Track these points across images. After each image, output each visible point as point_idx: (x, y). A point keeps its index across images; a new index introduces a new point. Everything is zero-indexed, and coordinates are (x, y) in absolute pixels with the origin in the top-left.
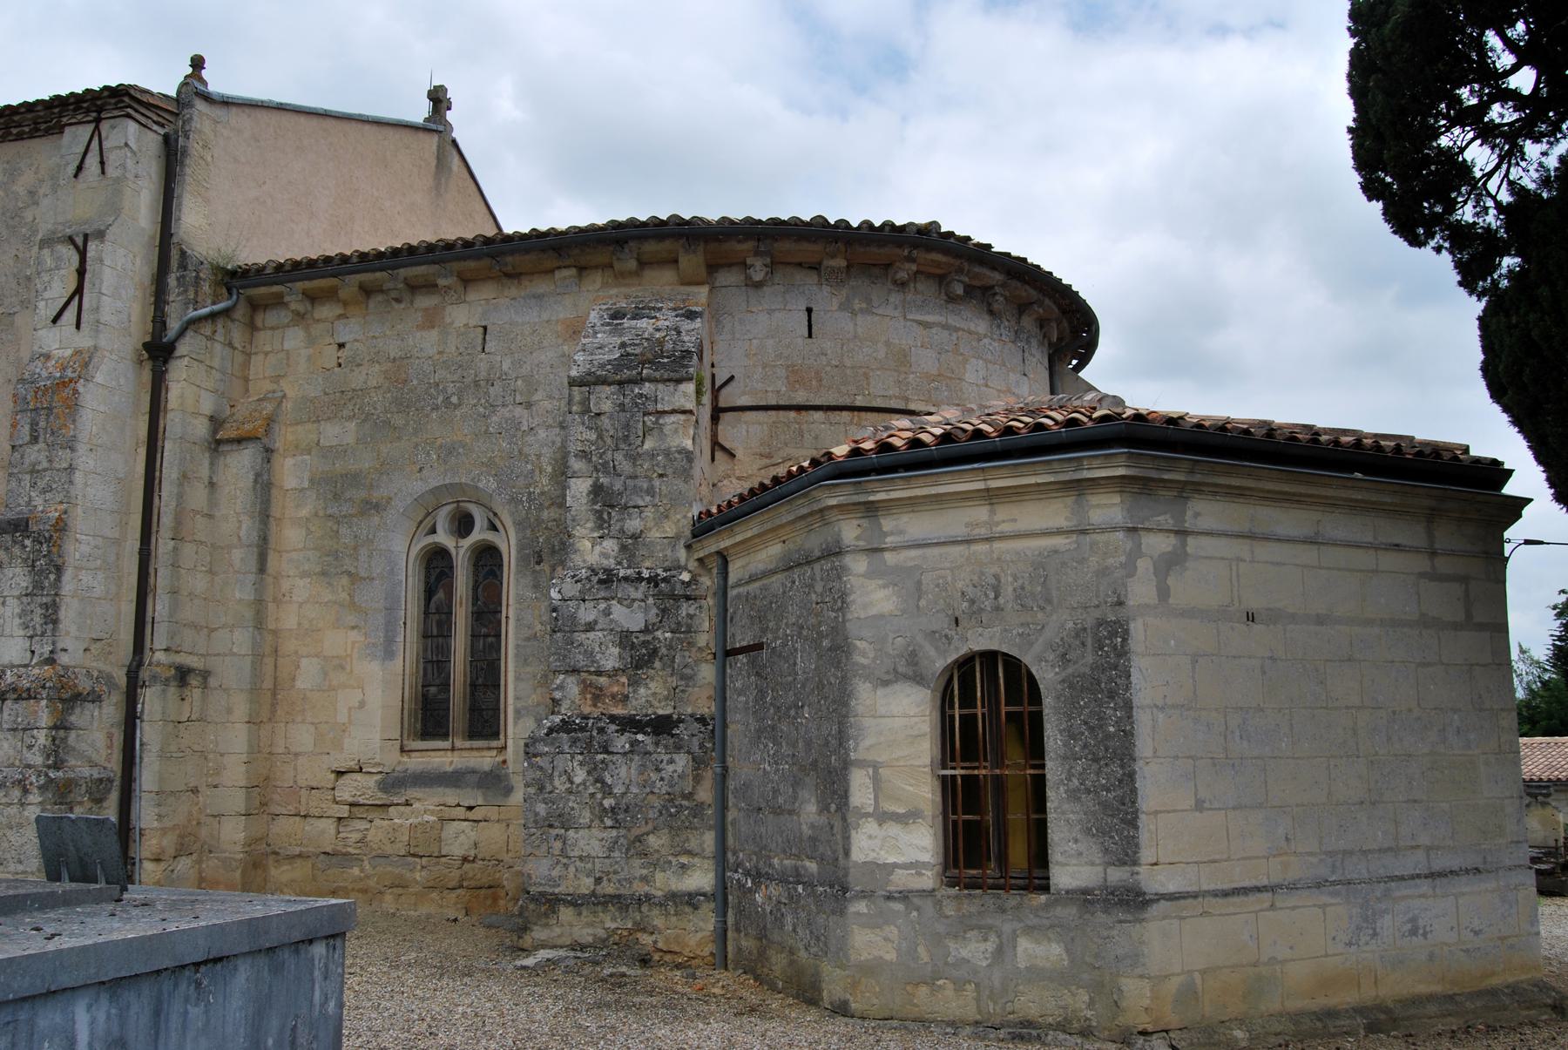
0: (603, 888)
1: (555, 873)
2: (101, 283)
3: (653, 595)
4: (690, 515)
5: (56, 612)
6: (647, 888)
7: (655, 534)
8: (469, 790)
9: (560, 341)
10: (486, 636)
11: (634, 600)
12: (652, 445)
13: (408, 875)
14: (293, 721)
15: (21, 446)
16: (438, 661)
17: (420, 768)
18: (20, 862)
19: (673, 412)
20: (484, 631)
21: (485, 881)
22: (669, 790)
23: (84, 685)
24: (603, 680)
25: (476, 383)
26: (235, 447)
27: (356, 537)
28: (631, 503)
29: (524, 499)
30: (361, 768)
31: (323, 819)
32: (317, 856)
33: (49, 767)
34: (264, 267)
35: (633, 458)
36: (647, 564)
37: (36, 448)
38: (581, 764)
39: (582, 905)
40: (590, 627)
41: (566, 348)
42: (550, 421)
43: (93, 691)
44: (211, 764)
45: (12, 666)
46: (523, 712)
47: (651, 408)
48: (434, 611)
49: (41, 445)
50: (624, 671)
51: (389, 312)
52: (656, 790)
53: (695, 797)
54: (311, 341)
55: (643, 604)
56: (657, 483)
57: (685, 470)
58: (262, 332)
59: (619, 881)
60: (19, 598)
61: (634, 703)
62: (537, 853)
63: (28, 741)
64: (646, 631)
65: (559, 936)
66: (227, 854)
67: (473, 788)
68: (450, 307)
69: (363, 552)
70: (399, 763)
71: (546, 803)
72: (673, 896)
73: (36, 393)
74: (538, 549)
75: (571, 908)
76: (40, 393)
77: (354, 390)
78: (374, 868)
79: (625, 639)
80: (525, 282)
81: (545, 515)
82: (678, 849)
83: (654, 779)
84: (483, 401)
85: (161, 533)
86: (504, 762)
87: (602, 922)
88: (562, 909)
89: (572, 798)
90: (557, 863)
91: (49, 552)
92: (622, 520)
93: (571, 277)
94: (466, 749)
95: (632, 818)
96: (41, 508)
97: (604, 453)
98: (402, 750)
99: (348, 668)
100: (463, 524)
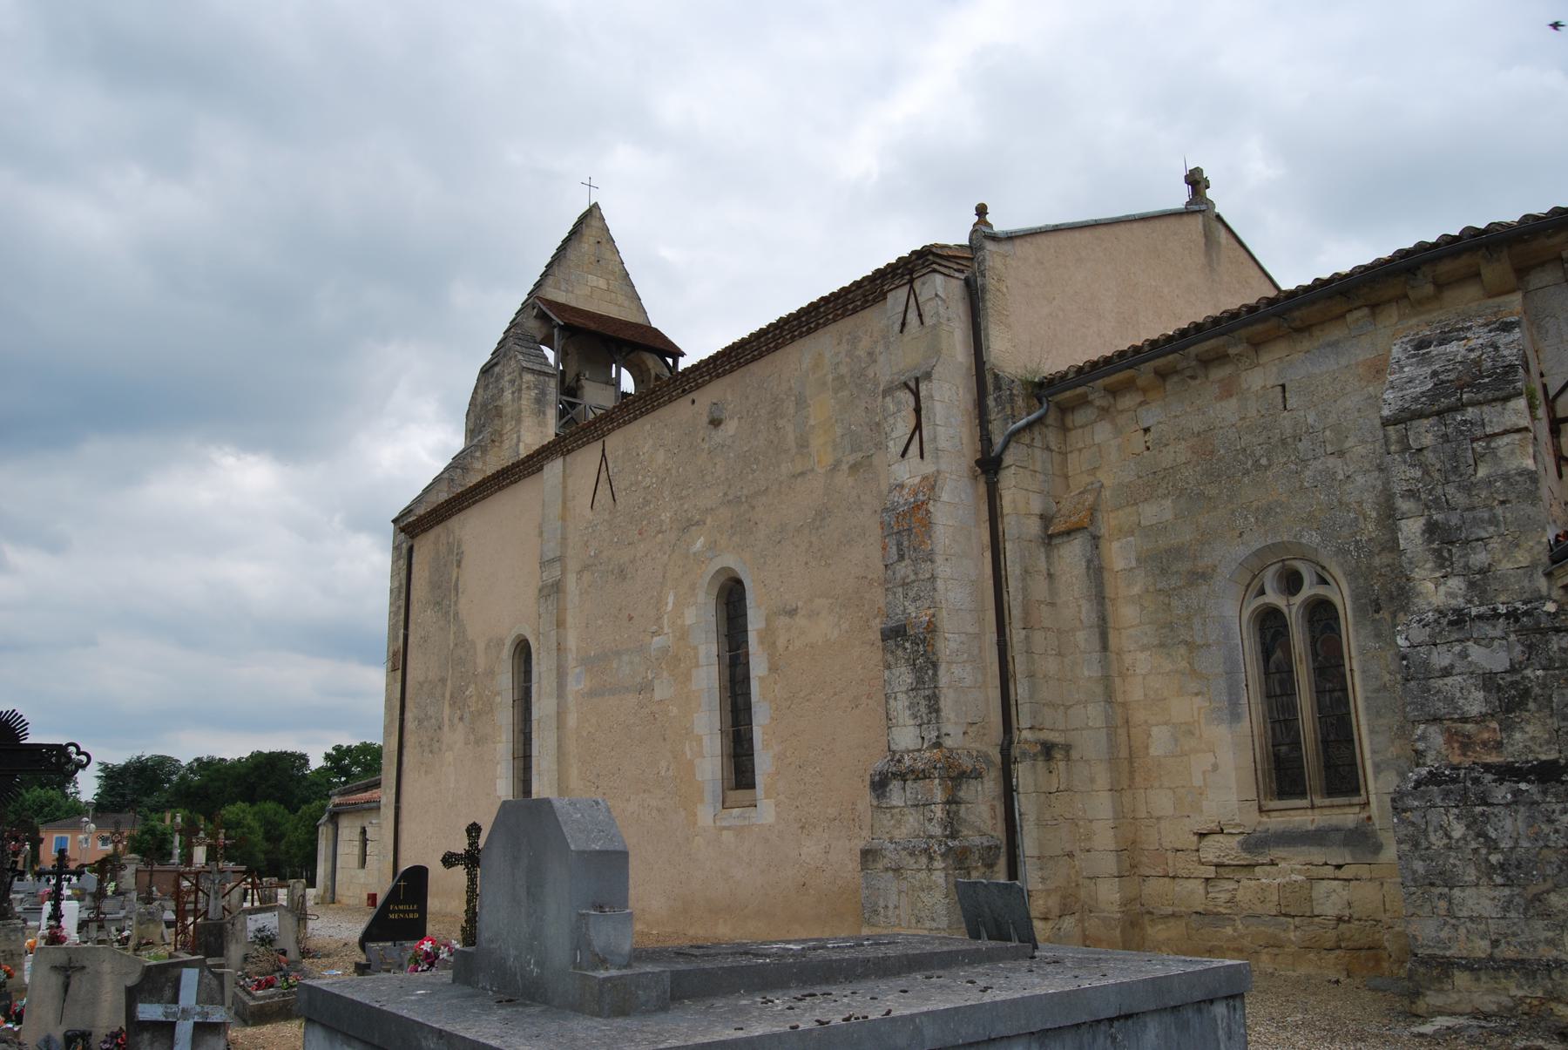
0: (1502, 952)
1: (1444, 934)
4: (1545, 540)
5: (937, 702)
9: (1364, 384)
10: (1332, 691)
11: (1493, 639)
14: (1152, 787)
18: (933, 920)
19: (1506, 432)
20: (1329, 686)
23: (967, 764)
24: (1469, 727)
25: (1283, 442)
26: (1065, 539)
27: (1187, 607)
28: (1473, 537)
29: (1352, 548)
30: (1222, 830)
31: (1191, 880)
32: (1190, 915)
33: (947, 837)
34: (1066, 373)
35: (1468, 488)
36: (1503, 598)
38: (1458, 818)
39: (1480, 969)
40: (1447, 672)
41: (1371, 389)
42: (1367, 466)
43: (975, 769)
44: (1081, 830)
45: (909, 751)
46: (1383, 766)
47: (1478, 433)
48: (1274, 671)
49: (907, 561)
50: (1492, 716)
52: (1551, 844)
54: (1118, 432)
55: (1504, 642)
56: (1499, 511)
57: (1530, 492)
61: (1510, 749)
62: (1420, 913)
63: (929, 815)
64: (1513, 669)
65: (1457, 1003)
66: (1105, 914)
70: (1259, 823)
71: (1424, 861)
74: (1374, 597)
75: (1467, 972)
76: (901, 518)
77: (1165, 469)
78: (1247, 927)
79: (1488, 681)
81: (1377, 561)
84: (1293, 458)
85: (1013, 624)
90: (1445, 924)
92: (1466, 555)
93: (1363, 317)
94: (1326, 807)
95: (1526, 874)
96: (914, 615)
97: (1433, 488)
98: (1261, 810)
99: (1197, 733)
100: (1292, 582)
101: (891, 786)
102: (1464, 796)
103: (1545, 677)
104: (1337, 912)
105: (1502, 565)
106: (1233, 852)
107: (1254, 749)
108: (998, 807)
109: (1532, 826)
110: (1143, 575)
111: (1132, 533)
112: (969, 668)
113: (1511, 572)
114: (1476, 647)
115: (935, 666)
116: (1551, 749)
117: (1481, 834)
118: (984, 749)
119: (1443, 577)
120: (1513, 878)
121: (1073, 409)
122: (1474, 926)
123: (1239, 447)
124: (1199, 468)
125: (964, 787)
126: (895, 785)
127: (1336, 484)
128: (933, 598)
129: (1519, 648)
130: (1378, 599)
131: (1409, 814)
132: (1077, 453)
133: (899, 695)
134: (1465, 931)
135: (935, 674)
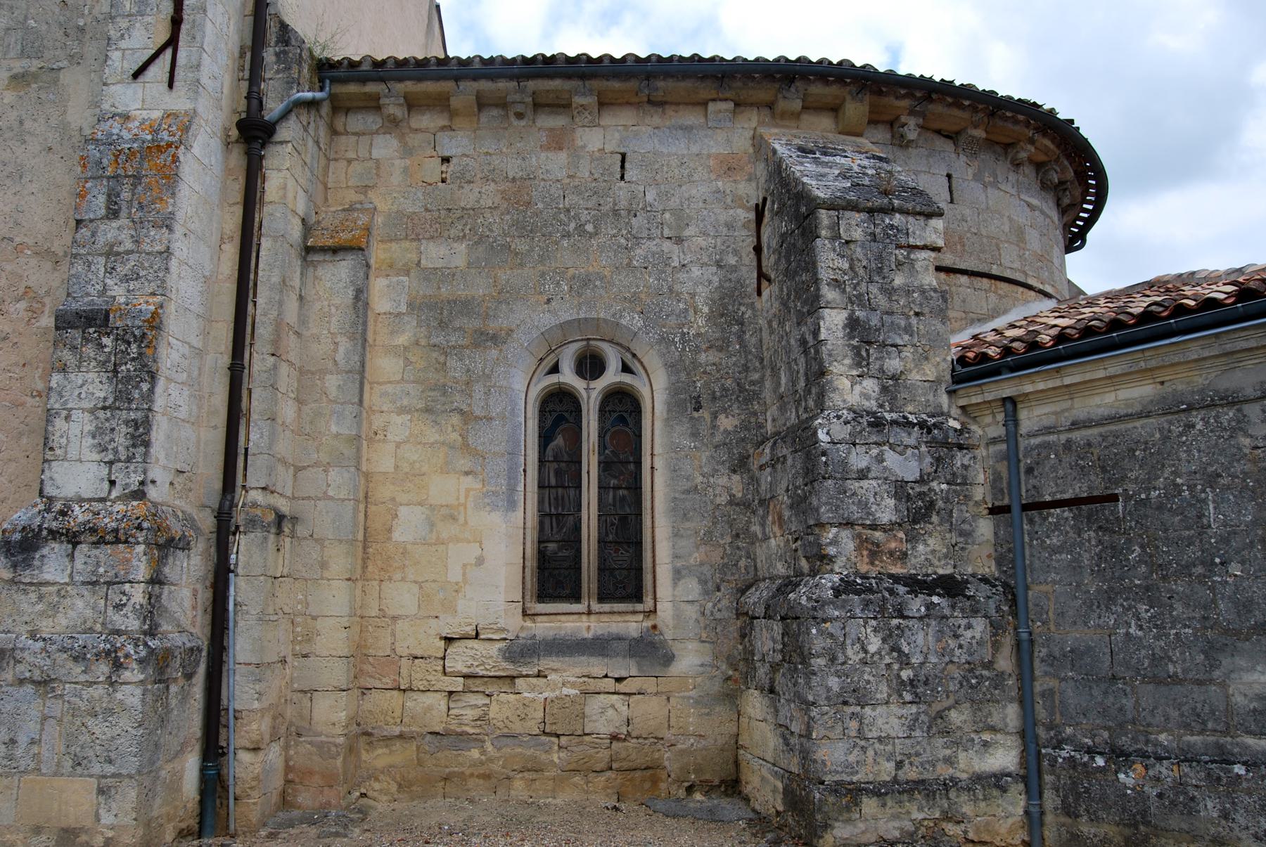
0: (906, 774)
1: (852, 758)
2: (204, 37)
3: (926, 442)
4: (949, 359)
5: (148, 432)
6: (951, 771)
7: (915, 377)
8: (620, 659)
9: (713, 177)
10: (616, 488)
11: (907, 447)
12: (903, 281)
13: (544, 756)
14: (390, 579)
15: (91, 221)
16: (558, 515)
17: (550, 634)
18: (110, 762)
19: (925, 247)
20: (613, 482)
21: (641, 761)
22: (969, 659)
23: (176, 529)
24: (878, 535)
25: (616, 213)
26: (328, 257)
27: (468, 370)
28: (889, 341)
29: (677, 339)
30: (477, 634)
31: (428, 693)
32: (423, 736)
33: (145, 633)
34: (359, 63)
35: (889, 292)
36: (910, 408)
37: (115, 224)
38: (875, 630)
39: (886, 794)
40: (863, 475)
41: (720, 184)
42: (705, 259)
43: (184, 536)
44: (299, 629)
45: (81, 500)
46: (684, 572)
47: (903, 241)
48: (551, 459)
49: (123, 221)
50: (900, 525)
51: (506, 129)
52: (956, 659)
53: (996, 666)
54: (407, 151)
55: (916, 451)
56: (914, 321)
57: (941, 310)
58: (344, 137)
59: (922, 764)
60: (92, 411)
61: (913, 561)
62: (831, 735)
63: (116, 598)
64: (921, 481)
65: (863, 832)
66: (323, 738)
67: (625, 657)
68: (580, 129)
69: (478, 389)
70: (522, 628)
71: (839, 677)
72: (978, 778)
73: (117, 157)
74: (695, 394)
75: (875, 798)
76: (123, 157)
77: (463, 209)
78: (499, 749)
79: (900, 489)
80: (670, 111)
81: (703, 357)
82: (981, 725)
83: (952, 646)
84: (624, 232)
85: (256, 347)
86: (654, 627)
87: (909, 813)
88: (865, 800)
89: (868, 669)
90: (854, 746)
91: (140, 354)
92: (882, 358)
93: (726, 110)
94: (605, 613)
95: (932, 691)
96: (122, 300)
97: (858, 284)
98: (525, 614)
99: (461, 520)
100: (591, 365)
101: (45, 551)
102: (883, 609)
103: (948, 491)
104: (612, 730)
105: (913, 375)
106: (490, 661)
107: (524, 544)
108: (200, 592)
109: (940, 641)
110: (415, 323)
111: (407, 273)
112: (186, 393)
113: (919, 383)
114: (892, 452)
115: (153, 377)
116: (948, 564)
117: (895, 649)
118: (189, 509)
119: (859, 376)
120: (920, 695)
121: (348, 111)
122: (882, 747)
123: (561, 206)
124: (508, 217)
125: (171, 560)
126: (54, 553)
127: (669, 270)
128: (163, 281)
129: (928, 460)
130: (699, 396)
131: (828, 625)
132: (345, 163)
133: (76, 415)
134: (872, 753)
135: (152, 390)
